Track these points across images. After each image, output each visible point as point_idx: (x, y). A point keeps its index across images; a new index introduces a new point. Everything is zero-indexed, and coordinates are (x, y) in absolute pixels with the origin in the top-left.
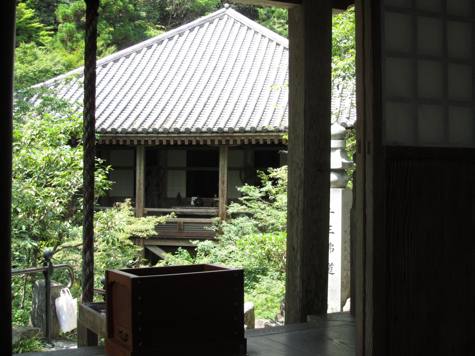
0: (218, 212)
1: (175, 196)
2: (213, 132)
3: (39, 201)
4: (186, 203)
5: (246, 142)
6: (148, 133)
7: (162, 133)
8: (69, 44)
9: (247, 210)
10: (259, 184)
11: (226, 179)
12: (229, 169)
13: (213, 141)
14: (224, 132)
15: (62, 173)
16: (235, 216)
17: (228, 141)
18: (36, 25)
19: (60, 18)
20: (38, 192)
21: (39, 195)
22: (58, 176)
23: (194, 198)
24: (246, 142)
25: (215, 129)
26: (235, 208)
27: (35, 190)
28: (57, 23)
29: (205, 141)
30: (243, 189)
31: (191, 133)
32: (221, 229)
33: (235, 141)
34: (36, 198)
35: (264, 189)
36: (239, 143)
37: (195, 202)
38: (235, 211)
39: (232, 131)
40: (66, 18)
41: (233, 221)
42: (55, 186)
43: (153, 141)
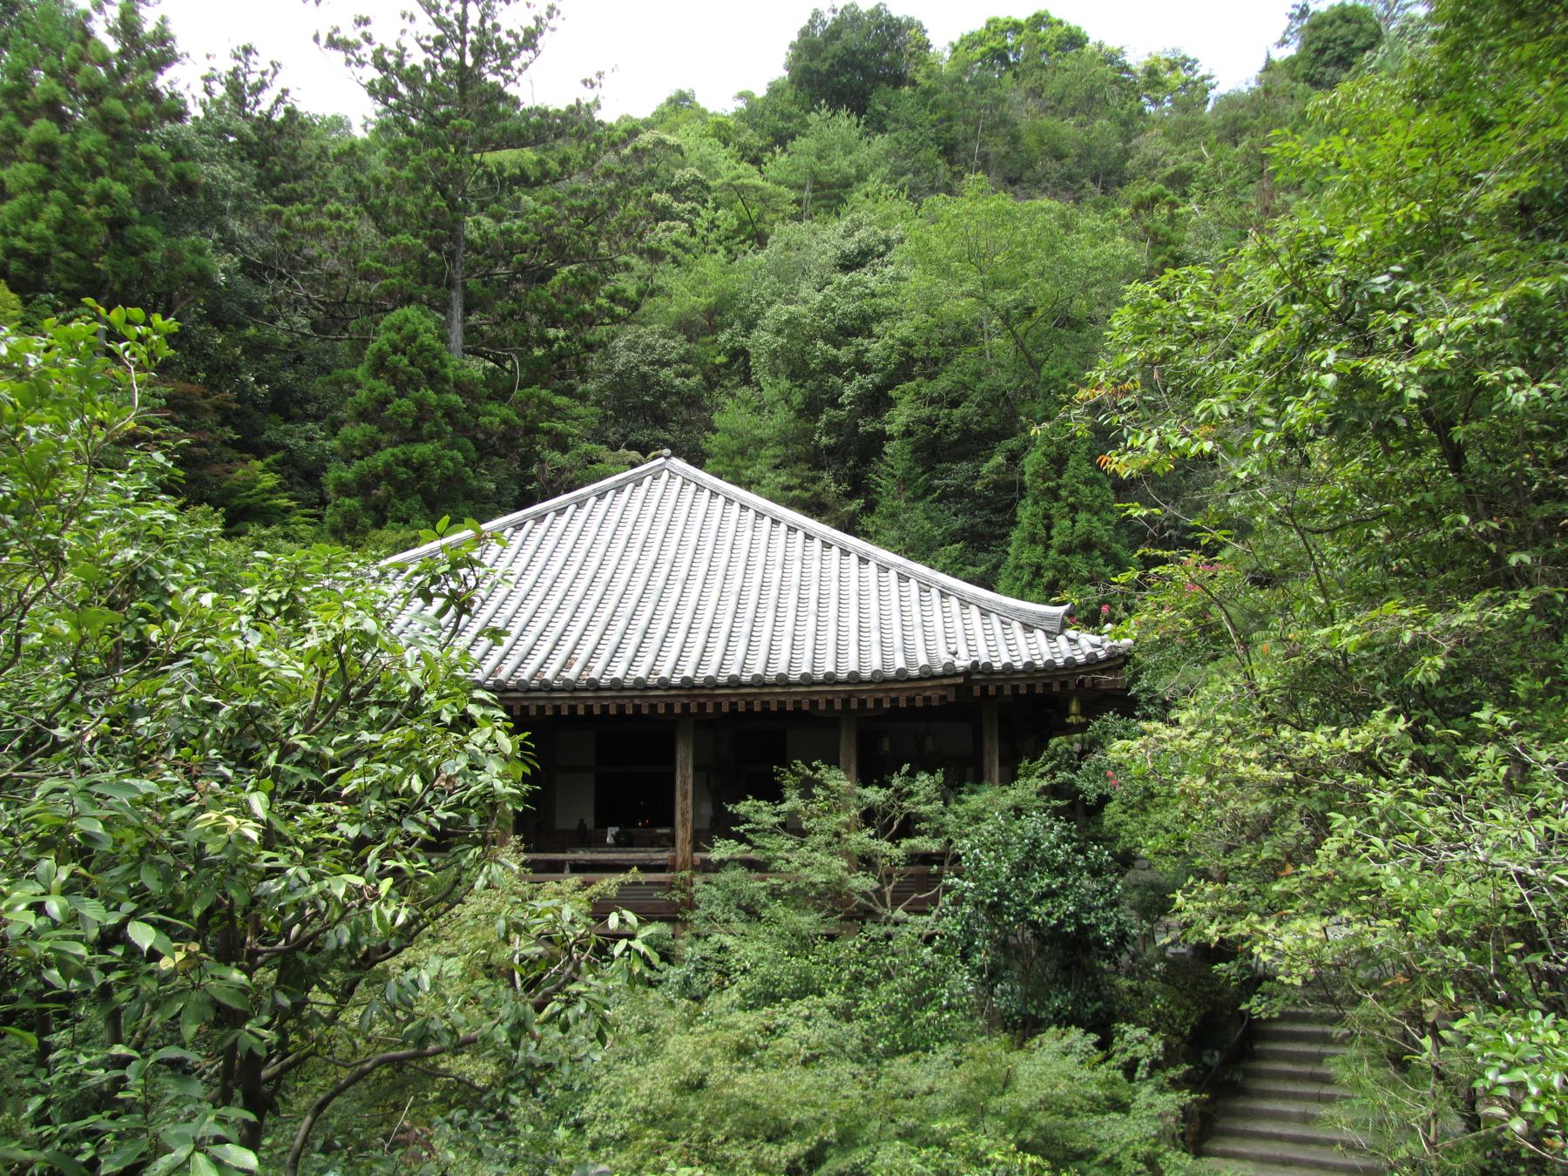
0: (674, 859)
1: (573, 825)
2: (672, 687)
3: (281, 870)
4: (597, 842)
5: (741, 708)
6: (530, 690)
7: (561, 690)
8: (347, 536)
9: (753, 855)
10: (774, 794)
11: (690, 787)
12: (696, 769)
13: (669, 707)
14: (695, 687)
15: (394, 739)
16: (721, 865)
17: (702, 706)
18: (284, 502)
19: (330, 489)
20: (278, 825)
21: (285, 841)
22: (371, 752)
23: (612, 831)
24: (741, 708)
25: (676, 681)
26: (722, 850)
27: (262, 815)
28: (324, 502)
29: (653, 707)
30: (743, 808)
31: (623, 689)
32: (691, 896)
33: (718, 706)
34: (268, 854)
35: (785, 807)
36: (725, 708)
37: (616, 837)
38: (725, 856)
39: (711, 683)
40: (343, 489)
41: (712, 876)
42: (352, 800)
43: (541, 709)
